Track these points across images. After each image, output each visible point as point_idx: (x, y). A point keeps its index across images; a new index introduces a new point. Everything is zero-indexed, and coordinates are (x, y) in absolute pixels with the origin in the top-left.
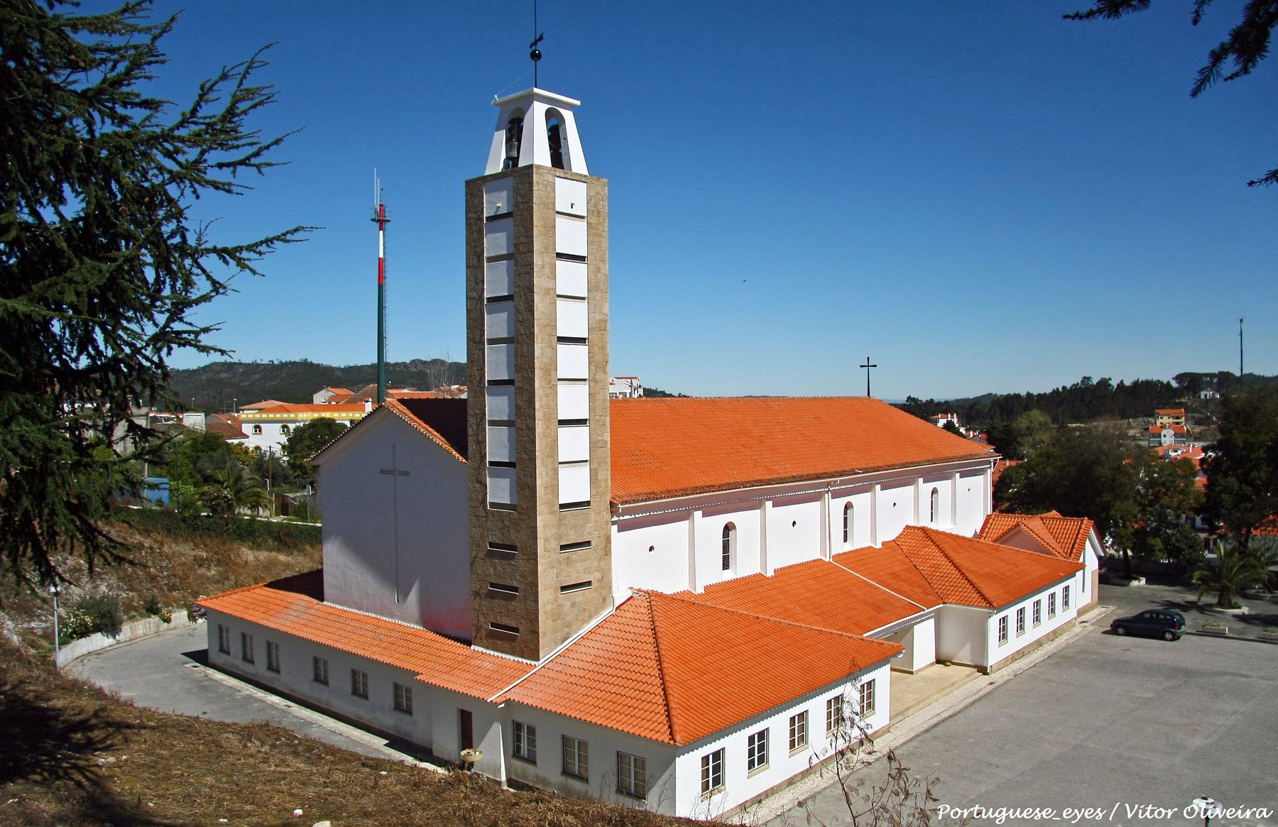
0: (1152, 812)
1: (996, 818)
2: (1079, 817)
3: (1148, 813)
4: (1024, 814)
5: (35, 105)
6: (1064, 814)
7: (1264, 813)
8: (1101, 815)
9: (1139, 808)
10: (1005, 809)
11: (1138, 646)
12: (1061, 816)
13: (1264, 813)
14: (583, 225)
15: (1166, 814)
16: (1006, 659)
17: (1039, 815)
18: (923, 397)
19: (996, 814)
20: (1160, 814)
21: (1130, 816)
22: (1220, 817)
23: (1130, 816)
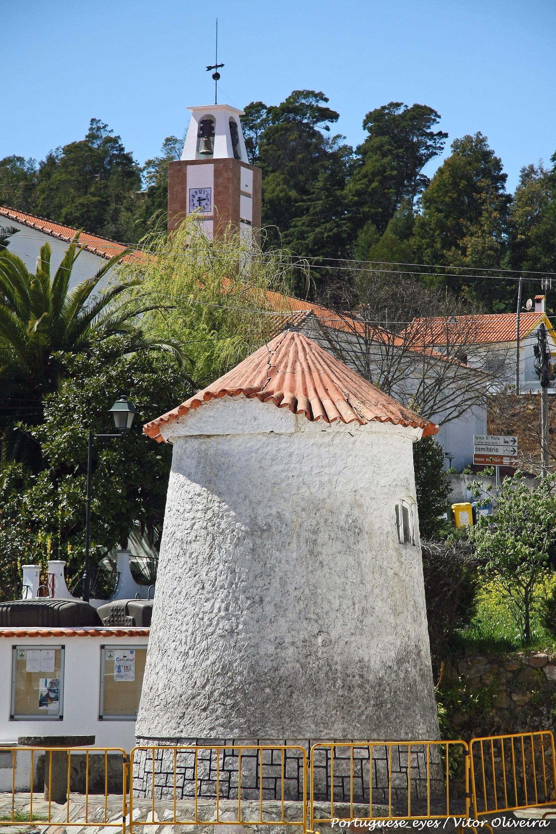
0: (471, 823)
1: (369, 827)
2: (423, 826)
3: (468, 824)
4: (388, 824)
5: (388, 365)
6: (414, 824)
7: (544, 824)
8: (437, 825)
9: (462, 820)
10: (374, 821)
11: (415, 607)
12: (412, 825)
13: (544, 824)
14: (251, 200)
15: (347, 824)
16: (29, 738)
17: (397, 825)
18: (395, 102)
19: (369, 824)
20: (476, 824)
21: (456, 825)
22: (515, 826)
23: (456, 825)
